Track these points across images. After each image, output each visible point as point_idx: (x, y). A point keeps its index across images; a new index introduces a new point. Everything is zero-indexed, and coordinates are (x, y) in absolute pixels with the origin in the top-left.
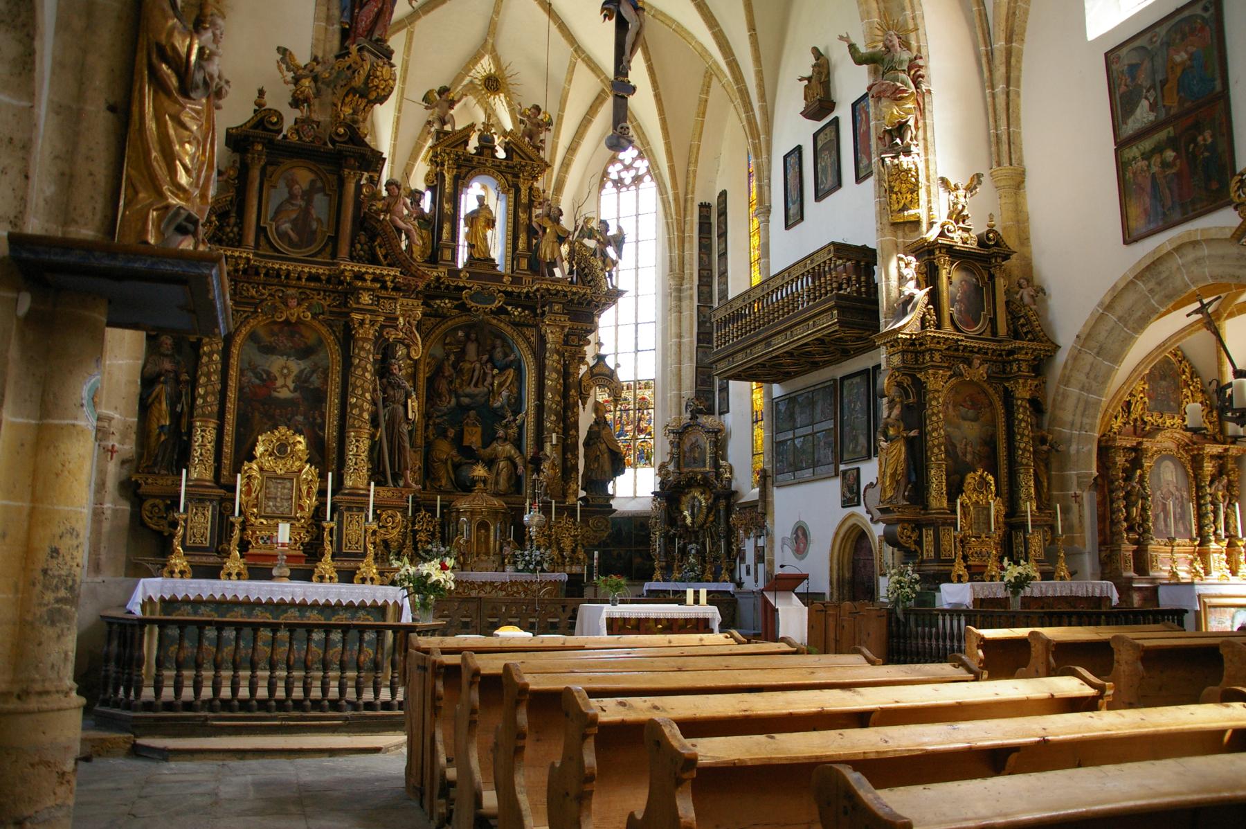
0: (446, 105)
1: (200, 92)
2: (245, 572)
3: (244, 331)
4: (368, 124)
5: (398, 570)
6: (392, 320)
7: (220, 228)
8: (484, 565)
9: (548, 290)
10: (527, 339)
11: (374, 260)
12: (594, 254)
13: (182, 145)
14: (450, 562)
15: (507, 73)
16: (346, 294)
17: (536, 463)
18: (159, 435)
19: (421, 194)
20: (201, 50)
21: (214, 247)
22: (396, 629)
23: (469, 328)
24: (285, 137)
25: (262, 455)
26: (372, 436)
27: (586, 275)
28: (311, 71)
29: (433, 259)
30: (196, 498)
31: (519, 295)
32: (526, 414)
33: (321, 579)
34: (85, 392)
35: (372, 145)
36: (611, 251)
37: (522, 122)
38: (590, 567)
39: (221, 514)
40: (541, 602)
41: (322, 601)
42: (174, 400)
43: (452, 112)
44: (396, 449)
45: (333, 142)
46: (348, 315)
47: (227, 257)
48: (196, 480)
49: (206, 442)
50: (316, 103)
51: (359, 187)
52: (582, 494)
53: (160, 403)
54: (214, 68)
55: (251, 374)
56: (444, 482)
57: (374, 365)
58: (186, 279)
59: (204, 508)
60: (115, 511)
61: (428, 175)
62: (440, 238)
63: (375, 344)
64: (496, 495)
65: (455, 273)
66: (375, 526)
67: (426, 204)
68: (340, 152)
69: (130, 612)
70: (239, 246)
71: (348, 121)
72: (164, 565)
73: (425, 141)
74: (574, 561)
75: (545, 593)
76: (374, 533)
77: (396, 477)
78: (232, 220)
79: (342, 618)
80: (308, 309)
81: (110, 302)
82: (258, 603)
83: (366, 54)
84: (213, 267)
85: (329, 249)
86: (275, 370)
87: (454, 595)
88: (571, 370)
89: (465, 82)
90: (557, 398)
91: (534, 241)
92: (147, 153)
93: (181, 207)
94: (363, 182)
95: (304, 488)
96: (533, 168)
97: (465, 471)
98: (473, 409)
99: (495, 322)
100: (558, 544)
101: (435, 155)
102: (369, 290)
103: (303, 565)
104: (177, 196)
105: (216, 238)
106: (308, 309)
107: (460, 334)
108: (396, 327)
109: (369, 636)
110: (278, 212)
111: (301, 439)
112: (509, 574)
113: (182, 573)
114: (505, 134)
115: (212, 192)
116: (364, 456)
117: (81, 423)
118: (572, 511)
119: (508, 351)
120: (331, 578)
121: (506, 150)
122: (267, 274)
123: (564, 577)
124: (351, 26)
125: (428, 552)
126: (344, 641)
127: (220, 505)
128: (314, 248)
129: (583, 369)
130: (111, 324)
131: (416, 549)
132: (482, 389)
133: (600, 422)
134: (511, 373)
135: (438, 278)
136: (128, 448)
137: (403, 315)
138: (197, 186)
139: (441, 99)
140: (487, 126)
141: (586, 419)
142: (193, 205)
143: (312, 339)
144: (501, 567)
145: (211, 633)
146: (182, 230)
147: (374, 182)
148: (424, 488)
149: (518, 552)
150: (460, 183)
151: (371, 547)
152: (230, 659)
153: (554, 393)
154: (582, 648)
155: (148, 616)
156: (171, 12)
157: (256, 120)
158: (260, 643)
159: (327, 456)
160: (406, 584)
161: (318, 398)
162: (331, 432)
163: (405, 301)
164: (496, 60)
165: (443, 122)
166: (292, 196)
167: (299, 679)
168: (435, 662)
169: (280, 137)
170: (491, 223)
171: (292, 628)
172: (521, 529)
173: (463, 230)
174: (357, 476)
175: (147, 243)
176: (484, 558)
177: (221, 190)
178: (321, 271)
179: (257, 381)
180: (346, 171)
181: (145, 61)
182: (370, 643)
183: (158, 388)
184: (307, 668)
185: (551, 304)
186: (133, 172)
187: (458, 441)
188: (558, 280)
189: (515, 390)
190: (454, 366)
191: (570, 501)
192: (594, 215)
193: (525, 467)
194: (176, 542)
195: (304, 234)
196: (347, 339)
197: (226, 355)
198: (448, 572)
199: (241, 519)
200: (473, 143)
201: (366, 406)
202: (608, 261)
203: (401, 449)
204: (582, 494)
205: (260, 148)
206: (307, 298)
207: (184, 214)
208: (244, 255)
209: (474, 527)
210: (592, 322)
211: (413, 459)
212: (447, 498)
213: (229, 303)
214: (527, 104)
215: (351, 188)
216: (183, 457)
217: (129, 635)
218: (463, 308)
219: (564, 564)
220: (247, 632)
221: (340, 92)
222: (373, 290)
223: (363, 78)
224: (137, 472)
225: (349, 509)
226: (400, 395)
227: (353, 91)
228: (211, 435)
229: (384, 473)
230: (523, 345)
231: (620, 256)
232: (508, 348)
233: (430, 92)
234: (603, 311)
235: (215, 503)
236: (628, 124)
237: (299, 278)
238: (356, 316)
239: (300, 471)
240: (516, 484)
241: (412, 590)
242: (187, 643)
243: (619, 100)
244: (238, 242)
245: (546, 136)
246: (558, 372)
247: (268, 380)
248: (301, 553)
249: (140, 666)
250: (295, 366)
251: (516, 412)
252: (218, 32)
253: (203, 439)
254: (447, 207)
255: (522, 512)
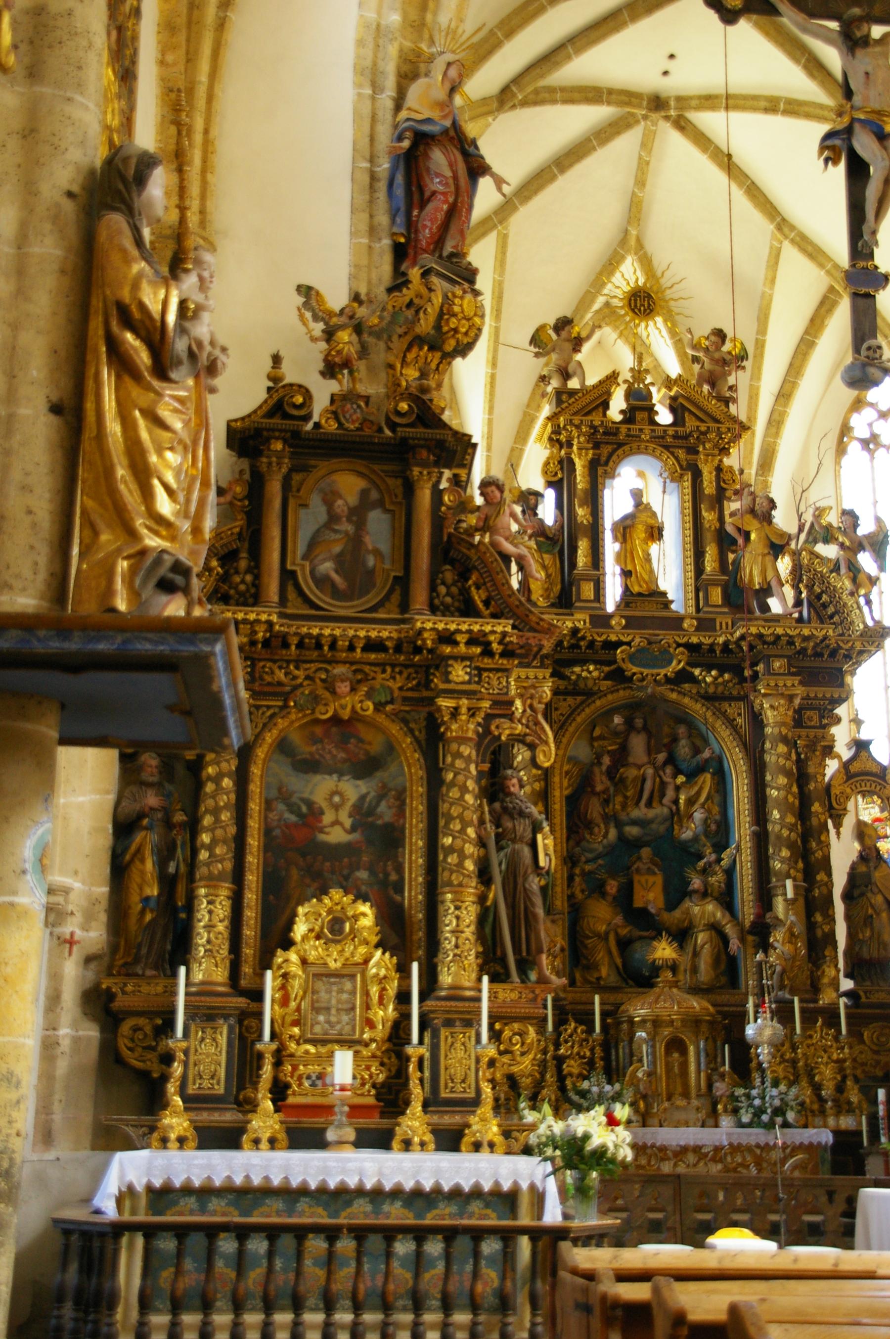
0: (568, 346)
1: (184, 369)
2: (282, 1136)
3: (269, 738)
4: (445, 391)
5: (533, 1127)
6: (503, 705)
7: (224, 578)
8: (681, 1116)
9: (760, 636)
10: (730, 722)
11: (468, 610)
12: (836, 569)
13: (160, 452)
14: (622, 1112)
15: (665, 282)
16: (428, 667)
17: (760, 933)
18: (143, 912)
19: (538, 495)
20: (183, 305)
21: (217, 608)
22: (536, 1234)
23: (631, 709)
24: (317, 425)
25: (305, 938)
26: (482, 899)
27: (825, 606)
28: (351, 317)
29: (565, 600)
30: (203, 1014)
31: (712, 648)
32: (738, 848)
33: (407, 1145)
34: (28, 850)
35: (454, 424)
36: (866, 560)
37: (695, 359)
38: (873, 1119)
39: (242, 1038)
40: (789, 1184)
41: (409, 1185)
42: (165, 855)
43: (578, 357)
44: (522, 918)
45: (393, 426)
46: (431, 701)
47: (237, 623)
48: (203, 983)
49: (215, 919)
50: (361, 367)
51: (437, 494)
52: (847, 984)
53: (143, 861)
54: (202, 330)
55: (281, 807)
56: (604, 971)
57: (478, 780)
58: (175, 660)
59: (215, 1029)
60: (76, 1040)
61: (547, 464)
62: (573, 565)
63: (478, 746)
64: (696, 990)
65: (601, 620)
66: (492, 1052)
67: (547, 512)
68: (404, 441)
69: (98, 1212)
70: (254, 605)
71: (413, 390)
72: (153, 1129)
73: (539, 408)
74: (843, 1107)
75: (794, 1167)
76: (492, 1063)
77: (524, 966)
78: (243, 564)
79: (443, 1215)
80: (369, 696)
81: (63, 706)
82: (303, 1191)
83: (435, 280)
84: (216, 641)
85: (396, 598)
86: (319, 798)
87: (632, 1170)
88: (811, 770)
89: (597, 306)
90: (790, 819)
91: (731, 557)
92: (109, 472)
93: (163, 551)
94: (444, 485)
95: (374, 990)
96: (719, 434)
97: (637, 950)
98: (647, 844)
99: (674, 696)
100: (811, 1076)
101: (557, 431)
102: (463, 658)
103: (375, 1122)
104: (157, 533)
105: (219, 595)
106: (369, 696)
107: (617, 720)
108: (510, 717)
109: (490, 1247)
110: (312, 544)
111: (365, 908)
112: (725, 1132)
113: (182, 1141)
114: (669, 383)
115: (209, 523)
116: (469, 932)
117: (22, 900)
118: (831, 1016)
119: (698, 742)
120: (423, 1144)
121: (672, 410)
122: (300, 645)
123: (826, 1137)
124: (408, 239)
125: (583, 1094)
126: (448, 1257)
127: (240, 1022)
128: (372, 599)
129: (832, 766)
130: (66, 740)
131: (562, 1089)
132: (659, 811)
133: (869, 856)
134: (706, 780)
135: (575, 631)
136: (94, 935)
137: (521, 696)
138: (186, 516)
139: (561, 337)
140: (638, 374)
141: (842, 852)
142: (182, 546)
143: (376, 745)
144: (712, 1119)
145: (227, 1245)
146: (166, 587)
147: (459, 483)
148: (572, 983)
149: (739, 1092)
150: (601, 469)
151: (487, 1090)
152: (259, 1291)
153: (785, 807)
154: (870, 1276)
155: (127, 1217)
156: (134, 252)
157: (271, 403)
158: (308, 1262)
159: (409, 936)
160: (549, 1151)
161: (390, 839)
162: (413, 895)
163: (523, 673)
164: (646, 262)
165: (566, 375)
166: (333, 518)
167: (372, 1327)
168: (604, 1298)
169: (310, 426)
170: (656, 533)
171: (360, 1233)
172: (743, 1054)
173: (611, 547)
174: (459, 968)
175: (113, 610)
176: (681, 1102)
177: (223, 517)
178: (385, 634)
179: (293, 818)
180: (416, 471)
181: (101, 332)
182: (491, 1260)
183: (139, 837)
184: (387, 1307)
185: (767, 659)
186: (90, 503)
187: (624, 900)
188: (777, 619)
189: (716, 809)
190: (611, 773)
191: (826, 998)
192: (831, 502)
193: (742, 940)
194: (171, 1088)
195: (356, 576)
196: (433, 740)
197: (242, 778)
198: (620, 1129)
199: (274, 1046)
200: (617, 405)
201: (469, 849)
202: (861, 577)
203: (530, 918)
204: (847, 984)
205: (278, 446)
206: (366, 679)
207: (168, 560)
208: (264, 617)
209: (661, 1049)
210: (842, 684)
211: (550, 934)
212: (612, 998)
213: (244, 694)
214: (702, 330)
215: (425, 496)
216: (179, 948)
217: (96, 1252)
218: (619, 676)
219: (823, 1112)
220: (287, 1242)
221: (399, 345)
222: (470, 658)
223: (432, 319)
224: (110, 974)
225: (449, 1023)
226: (523, 828)
227: (419, 341)
228: (223, 909)
229: (503, 960)
230: (724, 732)
231: (882, 568)
232: (699, 740)
233: (541, 329)
234: (859, 663)
235: (232, 1021)
236: (881, 340)
237: (351, 648)
238: (445, 703)
239: (366, 962)
240: (729, 970)
241: (559, 1162)
242: (189, 1264)
243: (861, 302)
244: (254, 598)
245: (738, 378)
246: (788, 774)
247: (311, 816)
248: (371, 1101)
249: (112, 1306)
250: (353, 790)
251: (721, 846)
252: (206, 274)
253: (211, 915)
254: (582, 513)
255: (741, 1019)
